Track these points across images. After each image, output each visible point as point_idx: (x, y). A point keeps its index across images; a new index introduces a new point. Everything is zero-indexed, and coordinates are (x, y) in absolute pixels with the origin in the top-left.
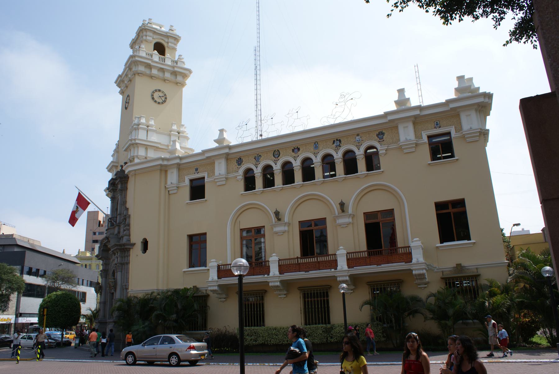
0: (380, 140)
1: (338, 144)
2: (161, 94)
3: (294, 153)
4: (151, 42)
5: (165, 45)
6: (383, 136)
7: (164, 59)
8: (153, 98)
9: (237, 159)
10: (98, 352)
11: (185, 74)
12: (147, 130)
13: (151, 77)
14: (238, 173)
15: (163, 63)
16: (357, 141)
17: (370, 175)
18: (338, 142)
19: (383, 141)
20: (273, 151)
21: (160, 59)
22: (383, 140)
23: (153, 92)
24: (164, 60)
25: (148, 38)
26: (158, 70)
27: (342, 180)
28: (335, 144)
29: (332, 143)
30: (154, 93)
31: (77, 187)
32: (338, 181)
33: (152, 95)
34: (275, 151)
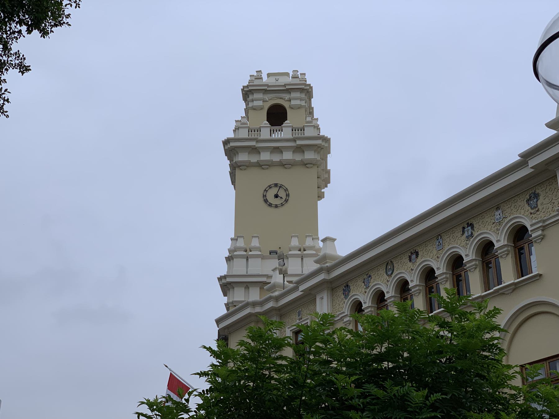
0: (532, 211)
1: (470, 233)
2: (274, 191)
3: (411, 263)
4: (262, 109)
5: (286, 105)
6: (537, 201)
8: (266, 201)
9: (344, 288)
10: (533, 386)
11: (317, 146)
12: (247, 257)
13: (260, 165)
14: (293, 330)
15: (303, 136)
16: (497, 219)
17: (520, 286)
18: (470, 228)
19: (538, 211)
20: (386, 264)
22: (537, 209)
23: (265, 190)
25: (293, 102)
26: (294, 152)
27: (511, 291)
28: (466, 234)
29: (461, 233)
30: (267, 191)
31: (166, 366)
32: (504, 294)
33: (264, 196)
34: (388, 263)
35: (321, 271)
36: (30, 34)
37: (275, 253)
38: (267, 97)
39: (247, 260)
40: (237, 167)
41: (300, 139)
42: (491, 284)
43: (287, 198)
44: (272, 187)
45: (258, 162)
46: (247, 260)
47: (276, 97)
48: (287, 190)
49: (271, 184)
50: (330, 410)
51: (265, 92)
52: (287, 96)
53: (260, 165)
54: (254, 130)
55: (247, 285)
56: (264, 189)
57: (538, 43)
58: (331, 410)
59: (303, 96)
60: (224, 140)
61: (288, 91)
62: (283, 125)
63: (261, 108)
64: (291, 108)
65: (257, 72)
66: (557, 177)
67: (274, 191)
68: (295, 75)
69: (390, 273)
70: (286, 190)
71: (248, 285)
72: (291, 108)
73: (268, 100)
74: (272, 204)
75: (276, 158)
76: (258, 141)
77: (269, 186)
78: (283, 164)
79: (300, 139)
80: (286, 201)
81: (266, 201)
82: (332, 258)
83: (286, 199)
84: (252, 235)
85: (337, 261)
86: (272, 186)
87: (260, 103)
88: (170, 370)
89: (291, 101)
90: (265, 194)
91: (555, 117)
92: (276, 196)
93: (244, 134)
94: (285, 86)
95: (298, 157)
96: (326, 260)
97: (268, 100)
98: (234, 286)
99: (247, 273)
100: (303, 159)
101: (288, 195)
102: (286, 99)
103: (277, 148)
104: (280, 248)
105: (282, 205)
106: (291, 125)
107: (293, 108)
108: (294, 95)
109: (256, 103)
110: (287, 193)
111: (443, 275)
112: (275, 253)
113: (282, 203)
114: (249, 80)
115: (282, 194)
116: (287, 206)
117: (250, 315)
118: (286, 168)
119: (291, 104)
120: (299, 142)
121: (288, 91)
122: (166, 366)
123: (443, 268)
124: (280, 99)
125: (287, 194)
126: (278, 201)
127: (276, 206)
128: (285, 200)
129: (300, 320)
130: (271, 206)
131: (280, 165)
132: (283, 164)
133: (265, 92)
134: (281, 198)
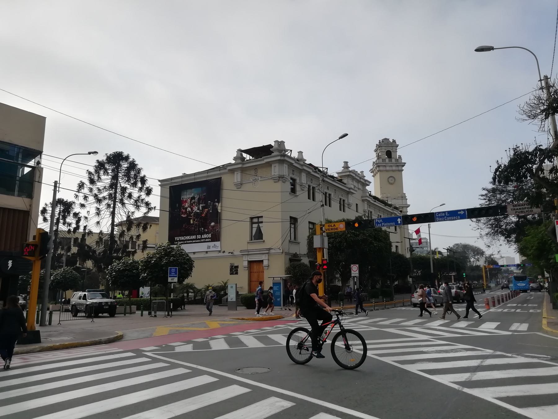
5: (391, 151)
13: (387, 171)
17: (184, 315)
36: (386, 140)
41: (398, 163)
42: (496, 305)
45: (398, 170)
50: (453, 275)
53: (387, 171)
57: (476, 47)
58: (135, 249)
63: (384, 152)
66: (328, 243)
75: (391, 168)
76: (386, 164)
78: (393, 171)
79: (398, 163)
87: (384, 150)
95: (397, 168)
103: (385, 166)
132: (393, 171)
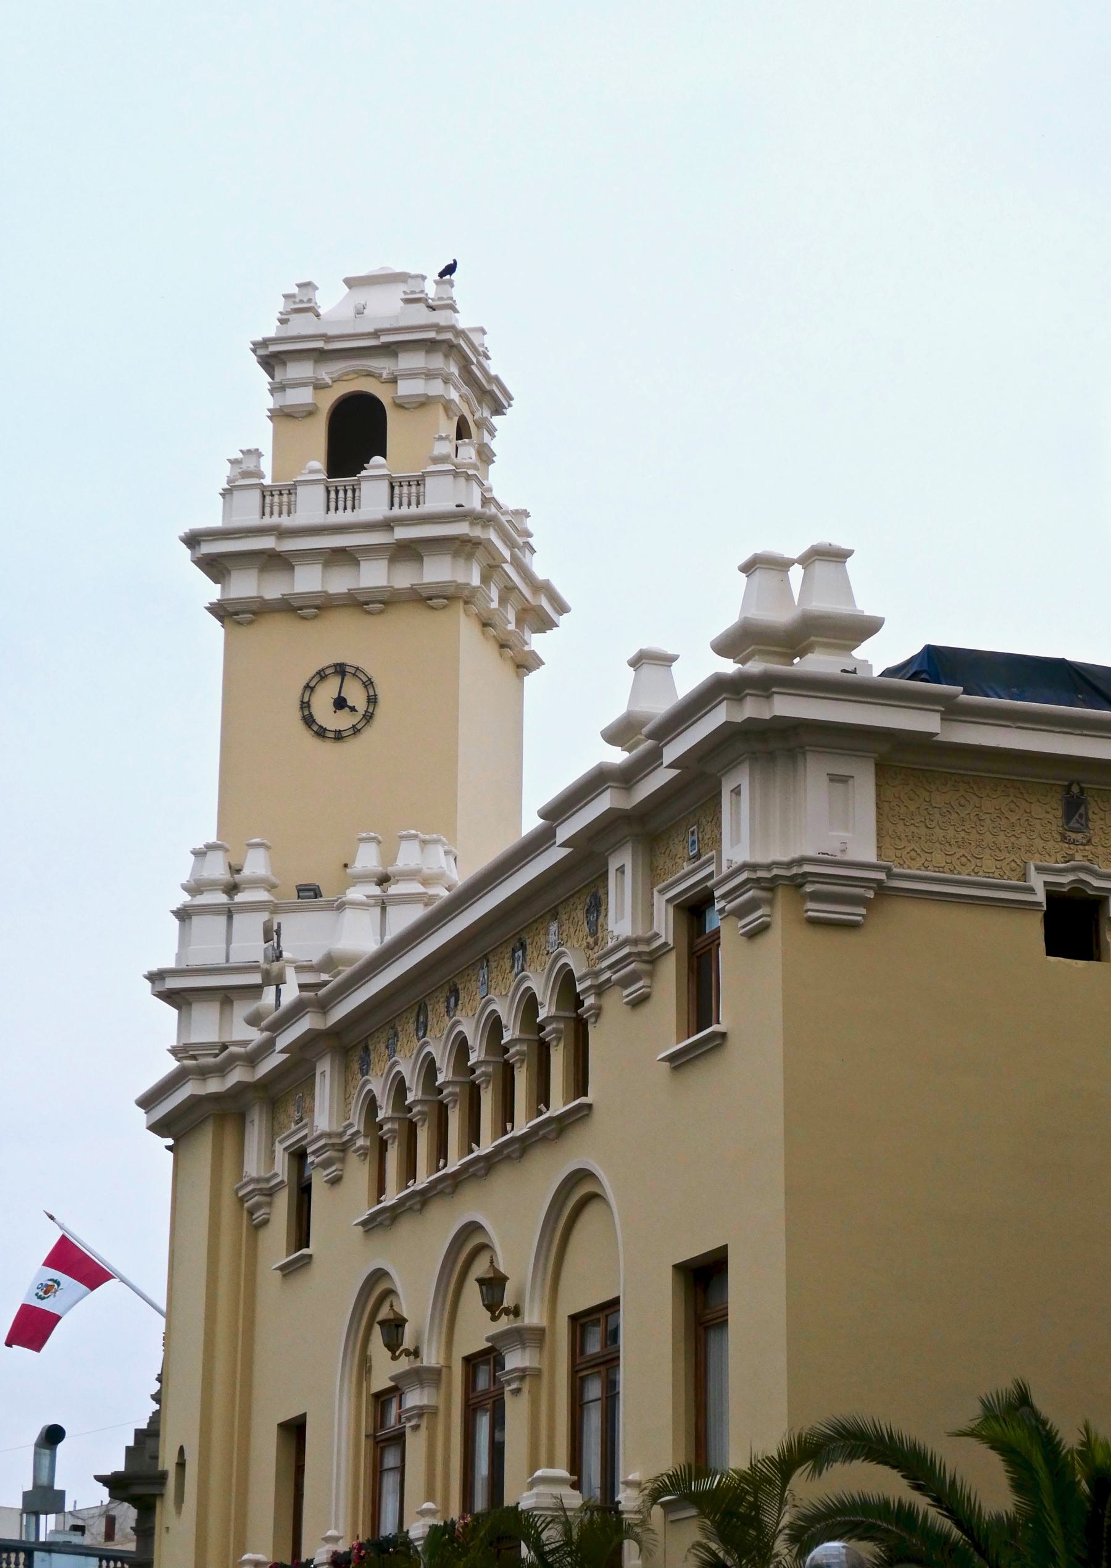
7: (354, 491)
21: (333, 495)
24: (350, 494)
25: (406, 388)
31: (52, 1217)
33: (305, 705)
35: (304, 1010)
37: (312, 893)
38: (326, 372)
39: (230, 918)
40: (227, 616)
43: (370, 710)
44: (326, 676)
46: (230, 918)
47: (354, 372)
48: (372, 683)
49: (307, 681)
51: (321, 356)
52: (383, 366)
54: (280, 491)
55: (227, 997)
56: (304, 684)
59: (437, 362)
60: (183, 535)
61: (390, 350)
62: (364, 473)
63: (310, 412)
64: (399, 406)
65: (299, 286)
67: (327, 692)
68: (413, 292)
69: (421, 1034)
70: (368, 684)
71: (229, 995)
72: (399, 406)
73: (330, 382)
74: (325, 729)
75: (339, 582)
77: (318, 673)
80: (368, 717)
81: (309, 721)
82: (347, 960)
83: (366, 711)
84: (247, 842)
85: (356, 966)
86: (328, 672)
88: (61, 1228)
89: (399, 381)
90: (306, 700)
91: (737, 620)
92: (340, 703)
93: (248, 513)
94: (376, 334)
96: (337, 967)
97: (330, 382)
98: (190, 1000)
99: (227, 961)
100: (415, 585)
101: (372, 700)
102: (384, 376)
104: (346, 866)
105: (356, 731)
106: (385, 472)
107: (406, 406)
108: (408, 361)
109: (303, 396)
110: (372, 693)
111: (481, 1066)
112: (312, 893)
113: (354, 726)
114: (281, 313)
115: (356, 695)
116: (370, 734)
117: (194, 1102)
118: (369, 613)
119: (399, 394)
120: (402, 533)
121: (390, 350)
122: (52, 1217)
123: (447, 1069)
124: (368, 375)
125: (368, 696)
126: (342, 721)
127: (339, 736)
128: (364, 716)
129: (298, 1123)
130: (324, 737)
131: (414, 601)
133: (321, 356)
134: (353, 709)
